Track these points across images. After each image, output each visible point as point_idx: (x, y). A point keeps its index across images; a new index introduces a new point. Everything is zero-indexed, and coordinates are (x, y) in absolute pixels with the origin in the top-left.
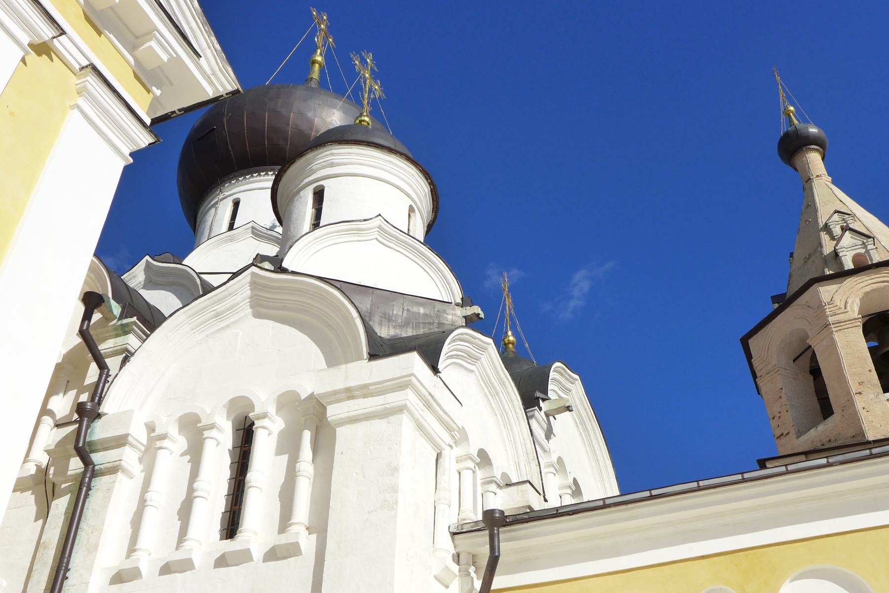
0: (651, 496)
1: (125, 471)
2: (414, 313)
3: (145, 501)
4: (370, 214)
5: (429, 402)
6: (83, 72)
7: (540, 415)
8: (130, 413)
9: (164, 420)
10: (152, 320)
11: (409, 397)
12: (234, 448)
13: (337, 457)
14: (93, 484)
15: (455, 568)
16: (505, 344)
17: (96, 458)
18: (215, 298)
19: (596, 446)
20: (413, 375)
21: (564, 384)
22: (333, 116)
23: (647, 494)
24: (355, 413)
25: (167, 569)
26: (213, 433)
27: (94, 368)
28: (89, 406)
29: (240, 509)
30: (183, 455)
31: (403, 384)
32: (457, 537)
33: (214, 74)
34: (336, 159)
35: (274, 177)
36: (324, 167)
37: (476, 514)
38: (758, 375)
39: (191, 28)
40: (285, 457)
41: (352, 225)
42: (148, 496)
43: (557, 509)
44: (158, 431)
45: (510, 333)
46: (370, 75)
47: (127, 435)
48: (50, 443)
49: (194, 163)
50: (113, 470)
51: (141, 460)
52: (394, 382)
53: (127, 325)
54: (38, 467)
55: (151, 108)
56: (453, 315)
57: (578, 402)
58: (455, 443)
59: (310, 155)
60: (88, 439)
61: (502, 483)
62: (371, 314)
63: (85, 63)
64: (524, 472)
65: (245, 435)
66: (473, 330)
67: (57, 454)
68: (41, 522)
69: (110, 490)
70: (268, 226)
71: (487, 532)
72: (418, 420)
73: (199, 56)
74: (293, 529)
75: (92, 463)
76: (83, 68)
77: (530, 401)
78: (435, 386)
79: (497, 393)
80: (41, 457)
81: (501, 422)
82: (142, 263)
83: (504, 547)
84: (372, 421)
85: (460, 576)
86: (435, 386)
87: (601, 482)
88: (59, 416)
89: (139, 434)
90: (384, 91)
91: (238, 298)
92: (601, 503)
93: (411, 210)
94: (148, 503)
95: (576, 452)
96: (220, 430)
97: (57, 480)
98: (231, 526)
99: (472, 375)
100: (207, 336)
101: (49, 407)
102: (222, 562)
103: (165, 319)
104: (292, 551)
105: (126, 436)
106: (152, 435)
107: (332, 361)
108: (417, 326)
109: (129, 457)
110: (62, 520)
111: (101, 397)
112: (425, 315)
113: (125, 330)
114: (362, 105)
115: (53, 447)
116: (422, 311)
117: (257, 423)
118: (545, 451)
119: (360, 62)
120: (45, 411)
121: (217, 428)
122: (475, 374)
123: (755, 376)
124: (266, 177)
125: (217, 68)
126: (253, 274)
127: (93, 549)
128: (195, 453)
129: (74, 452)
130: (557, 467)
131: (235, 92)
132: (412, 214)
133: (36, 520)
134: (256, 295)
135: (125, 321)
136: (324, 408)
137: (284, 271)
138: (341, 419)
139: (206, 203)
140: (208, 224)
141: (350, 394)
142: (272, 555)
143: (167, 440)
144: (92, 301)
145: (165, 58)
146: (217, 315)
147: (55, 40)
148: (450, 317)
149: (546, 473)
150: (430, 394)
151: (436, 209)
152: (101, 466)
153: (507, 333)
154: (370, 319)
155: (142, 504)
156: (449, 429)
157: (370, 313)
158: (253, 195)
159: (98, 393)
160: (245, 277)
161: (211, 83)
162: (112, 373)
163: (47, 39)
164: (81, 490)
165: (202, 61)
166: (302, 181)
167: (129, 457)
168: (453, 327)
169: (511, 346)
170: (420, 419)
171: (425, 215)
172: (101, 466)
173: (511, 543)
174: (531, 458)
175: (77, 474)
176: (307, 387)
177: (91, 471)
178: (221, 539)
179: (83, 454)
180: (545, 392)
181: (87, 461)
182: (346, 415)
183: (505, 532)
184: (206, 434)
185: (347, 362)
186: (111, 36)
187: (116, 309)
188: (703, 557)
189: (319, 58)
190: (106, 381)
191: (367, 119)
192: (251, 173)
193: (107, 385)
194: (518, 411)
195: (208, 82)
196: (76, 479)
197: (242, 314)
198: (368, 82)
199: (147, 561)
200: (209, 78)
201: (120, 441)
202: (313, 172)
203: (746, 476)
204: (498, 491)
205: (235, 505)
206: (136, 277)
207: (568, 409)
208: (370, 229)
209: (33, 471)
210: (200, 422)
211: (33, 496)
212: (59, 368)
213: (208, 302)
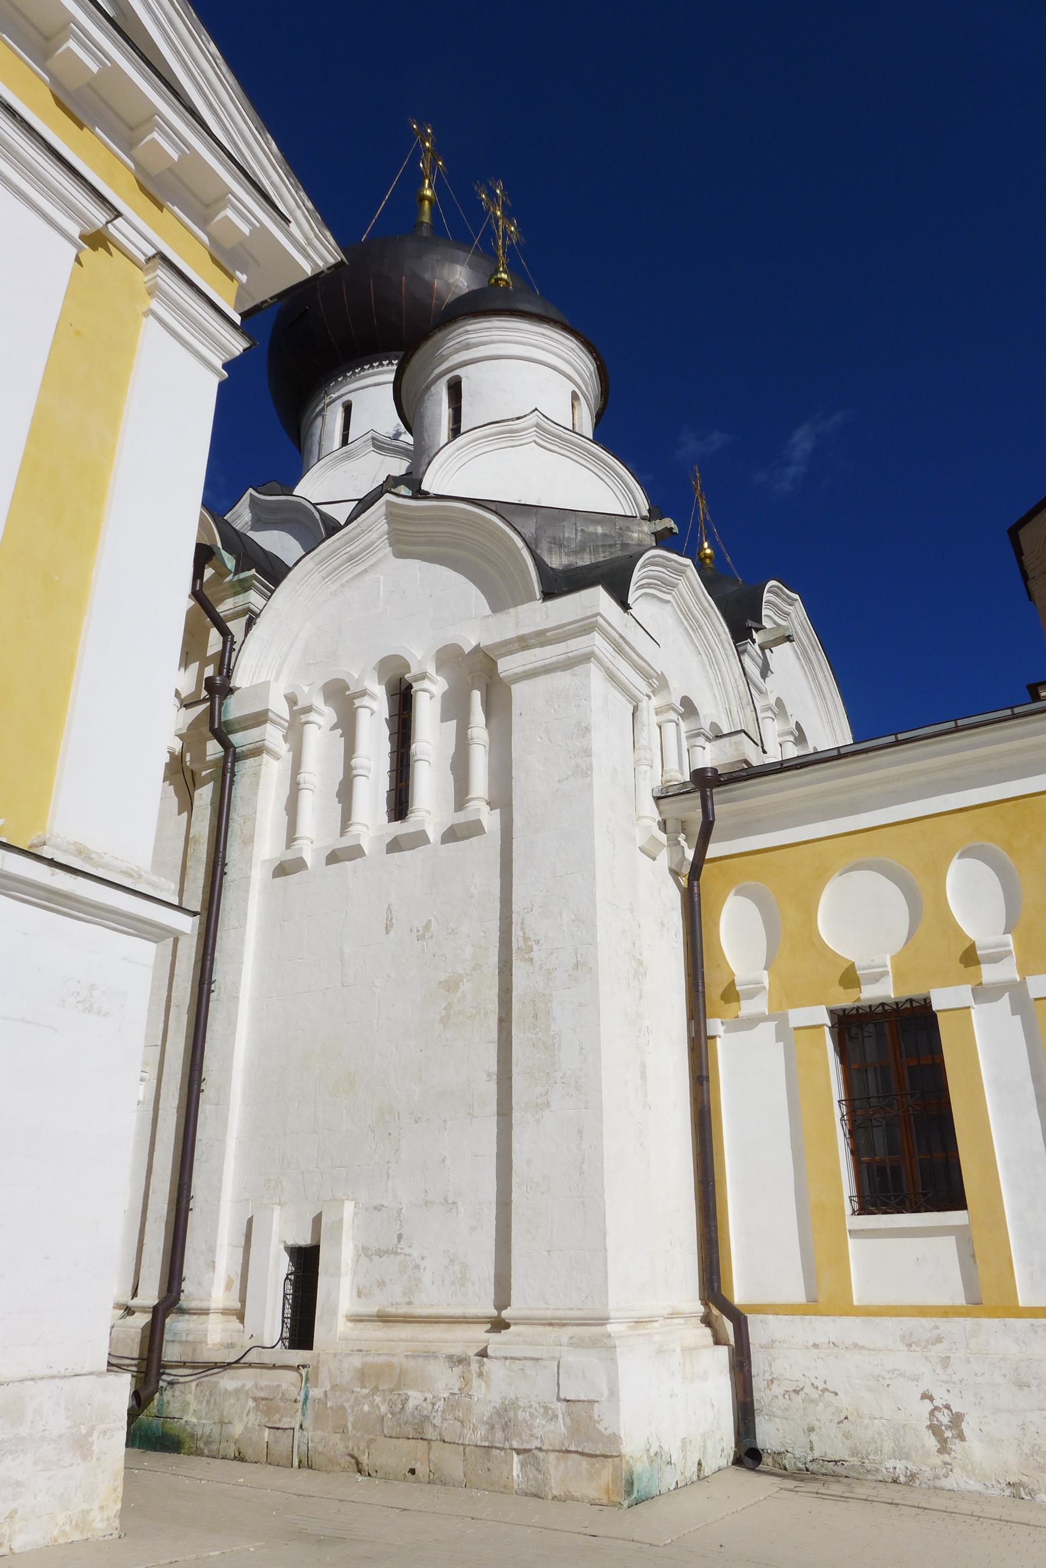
0: (897, 741)
1: (270, 752)
2: (590, 534)
3: (298, 784)
4: (524, 407)
5: (620, 645)
6: (150, 264)
7: (754, 649)
8: (266, 685)
9: (306, 689)
10: (274, 572)
11: (597, 642)
12: (391, 716)
14: (236, 769)
15: (663, 837)
16: (701, 560)
17: (236, 739)
18: (346, 538)
20: (599, 614)
21: (782, 608)
22: (459, 277)
23: (892, 739)
24: (531, 666)
25: (333, 858)
26: (366, 701)
27: (214, 635)
29: (407, 786)
30: (332, 729)
32: (661, 801)
33: (310, 244)
34: (473, 338)
36: (457, 351)
37: (682, 774)
38: (1031, 575)
39: (272, 183)
40: (453, 724)
41: (505, 428)
42: (301, 778)
43: (781, 763)
44: (302, 704)
45: (706, 545)
46: (502, 213)
47: (267, 711)
50: (258, 751)
53: (245, 579)
56: (639, 532)
57: (798, 627)
58: (653, 692)
59: (438, 336)
60: (223, 719)
61: (710, 735)
62: (537, 540)
63: (151, 252)
64: (737, 720)
67: (191, 738)
68: (185, 815)
69: (257, 774)
70: (391, 432)
73: (287, 221)
74: (473, 805)
75: (233, 746)
79: (700, 627)
81: (707, 663)
82: (246, 499)
83: (720, 810)
84: (553, 675)
85: (669, 846)
87: (829, 726)
89: (280, 708)
91: (373, 536)
92: (835, 753)
93: (575, 397)
95: (800, 694)
96: (373, 697)
97: (194, 767)
98: (400, 804)
99: (668, 607)
100: (342, 585)
102: (395, 846)
103: (289, 569)
104: (474, 829)
105: (267, 711)
106: (295, 708)
107: (498, 604)
108: (595, 551)
109: (273, 735)
110: (209, 811)
111: (229, 669)
112: (605, 535)
113: (244, 587)
114: (496, 258)
116: (600, 530)
117: (416, 686)
118: (761, 692)
122: (670, 613)
123: (1025, 578)
124: (380, 369)
125: (312, 235)
126: (389, 503)
127: (249, 841)
130: (776, 710)
131: (341, 263)
132: (576, 403)
133: (180, 813)
134: (395, 529)
135: (243, 575)
137: (425, 495)
138: (516, 674)
140: (316, 438)
141: (523, 644)
142: (452, 835)
146: (350, 559)
147: (109, 225)
148: (635, 535)
149: (764, 718)
150: (621, 636)
153: (702, 544)
154: (537, 547)
156: (646, 676)
157: (536, 539)
158: (370, 397)
159: (225, 664)
160: (379, 508)
161: (308, 257)
162: (238, 637)
163: (101, 225)
164: (225, 776)
165: (293, 228)
166: (432, 372)
167: (273, 735)
168: (641, 549)
169: (708, 561)
170: (612, 667)
171: (592, 402)
173: (726, 806)
174: (744, 701)
175: (217, 759)
176: (470, 639)
177: (232, 756)
178: (390, 821)
179: (221, 733)
180: (759, 620)
181: (226, 745)
182: (521, 669)
183: (718, 793)
185: (516, 604)
186: (175, 209)
187: (230, 562)
188: (961, 810)
189: (428, 193)
190: (232, 650)
191: (504, 276)
192: (361, 366)
193: (234, 654)
194: (727, 645)
197: (380, 555)
198: (500, 223)
199: (310, 850)
200: (305, 250)
201: (260, 719)
202: (445, 358)
203: (1017, 710)
204: (707, 745)
205: (401, 782)
206: (241, 516)
207: (789, 639)
208: (525, 429)
213: (338, 544)
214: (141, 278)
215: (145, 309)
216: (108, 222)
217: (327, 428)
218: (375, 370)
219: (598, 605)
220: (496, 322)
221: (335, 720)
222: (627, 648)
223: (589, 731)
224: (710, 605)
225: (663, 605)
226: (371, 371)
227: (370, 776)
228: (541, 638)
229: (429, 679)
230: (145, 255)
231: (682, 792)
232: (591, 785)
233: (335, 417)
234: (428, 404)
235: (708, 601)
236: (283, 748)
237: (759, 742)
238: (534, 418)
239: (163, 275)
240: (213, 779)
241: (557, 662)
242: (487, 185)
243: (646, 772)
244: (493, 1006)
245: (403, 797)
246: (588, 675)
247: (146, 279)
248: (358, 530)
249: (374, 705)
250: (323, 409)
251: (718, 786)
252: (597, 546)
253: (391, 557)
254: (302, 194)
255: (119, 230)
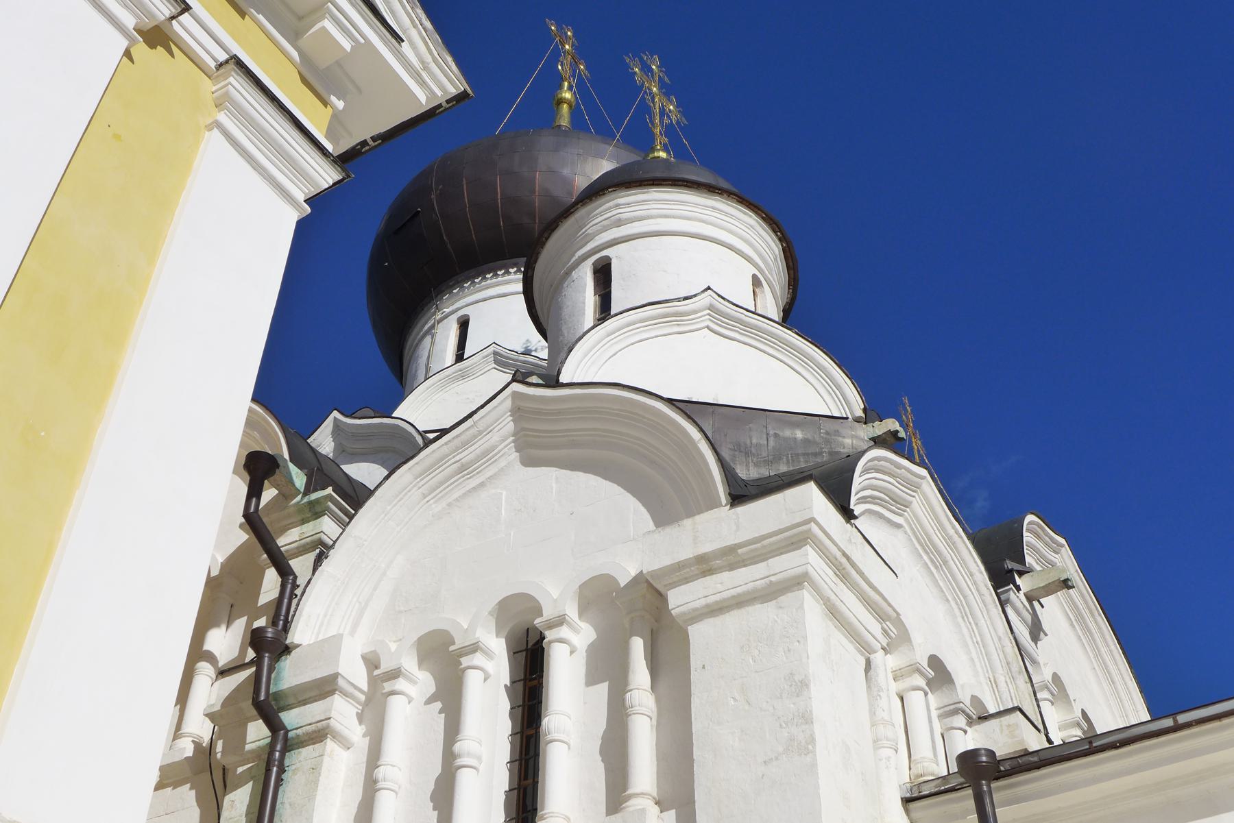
1: (337, 736)
2: (786, 439)
4: (690, 290)
5: (843, 569)
6: (222, 70)
7: (1018, 599)
8: (338, 638)
10: (356, 496)
11: (810, 559)
12: (513, 682)
13: (695, 675)
14: (287, 762)
18: (457, 442)
19: (1107, 658)
20: (813, 520)
21: (1046, 550)
24: (718, 597)
26: (478, 659)
27: (271, 577)
28: (270, 633)
30: (430, 701)
31: (797, 537)
32: (913, 805)
33: (426, 68)
35: (521, 276)
36: (606, 229)
40: (603, 688)
41: (668, 310)
42: (380, 773)
44: (385, 666)
46: (660, 89)
47: (335, 676)
48: (212, 702)
49: (397, 252)
50: (319, 735)
51: (360, 718)
52: (782, 536)
53: (317, 501)
54: (197, 745)
55: (336, 124)
56: (852, 437)
60: (273, 689)
61: (974, 714)
63: (223, 57)
64: (1006, 695)
65: (530, 660)
66: (896, 453)
67: (226, 719)
69: (316, 770)
71: (970, 791)
72: (829, 599)
73: (399, 39)
74: (635, 804)
75: (284, 727)
76: (221, 65)
77: (1001, 578)
78: (850, 541)
79: (945, 562)
80: (199, 727)
81: (958, 613)
82: (329, 422)
84: (750, 609)
86: (850, 541)
88: (222, 662)
89: (354, 673)
90: (683, 113)
91: (495, 437)
93: (756, 282)
94: (380, 785)
96: (488, 654)
97: (228, 761)
99: (900, 533)
100: (449, 505)
101: (206, 647)
105: (335, 676)
106: (376, 672)
107: (664, 516)
109: (342, 713)
112: (806, 441)
113: (315, 511)
115: (218, 707)
117: (550, 635)
119: (641, 70)
120: (197, 653)
121: (482, 650)
122: (907, 532)
124: (506, 278)
125: (429, 59)
126: (515, 395)
128: (450, 696)
129: (255, 712)
130: (1055, 689)
131: (461, 97)
132: (757, 290)
134: (524, 429)
135: (314, 496)
136: (661, 597)
139: (416, 330)
140: (422, 361)
143: (400, 679)
144: (258, 468)
145: (347, 45)
148: (848, 441)
150: (844, 554)
151: (794, 282)
152: (299, 732)
155: (371, 788)
156: (881, 616)
158: (494, 310)
159: (282, 612)
161: (422, 84)
162: (301, 581)
164: (270, 771)
167: (342, 713)
170: (833, 597)
172: (298, 732)
176: (626, 569)
177: (283, 743)
181: (275, 726)
182: (703, 602)
183: (1000, 789)
184: (465, 661)
185: (690, 514)
186: (261, 17)
187: (299, 478)
189: (568, 95)
190: (293, 595)
192: (482, 274)
193: (295, 602)
194: (984, 590)
195: (417, 82)
196: (259, 756)
197: (502, 463)
198: (656, 100)
200: (419, 75)
201: (325, 688)
202: (591, 237)
205: (526, 778)
206: (323, 441)
208: (695, 312)
209: (189, 752)
210: (453, 643)
211: (193, 792)
212: (212, 584)
213: (446, 450)
214: (208, 86)
215: (210, 121)
216: (173, 18)
217: (437, 348)
218: (500, 279)
219: (810, 508)
220: (655, 194)
221: (432, 689)
222: (853, 572)
223: (807, 686)
224: (957, 532)
225: (895, 531)
226: (494, 280)
227: (481, 768)
228: (731, 558)
229: (570, 625)
230: (215, 59)
231: (944, 789)
232: (814, 765)
233: (448, 335)
234: (569, 292)
235: (954, 527)
236: (356, 732)
237: (1041, 727)
238: (706, 299)
239: (236, 84)
240: (252, 778)
241: (755, 591)
242: (641, 60)
243: (888, 759)
244: (930, 743)
245: (529, 802)
246: (801, 607)
247: (214, 89)
248: (474, 431)
249: (489, 666)
250: (433, 327)
251: (997, 779)
252: (798, 455)
253: (518, 466)
254: (420, 11)
255: (185, 27)
